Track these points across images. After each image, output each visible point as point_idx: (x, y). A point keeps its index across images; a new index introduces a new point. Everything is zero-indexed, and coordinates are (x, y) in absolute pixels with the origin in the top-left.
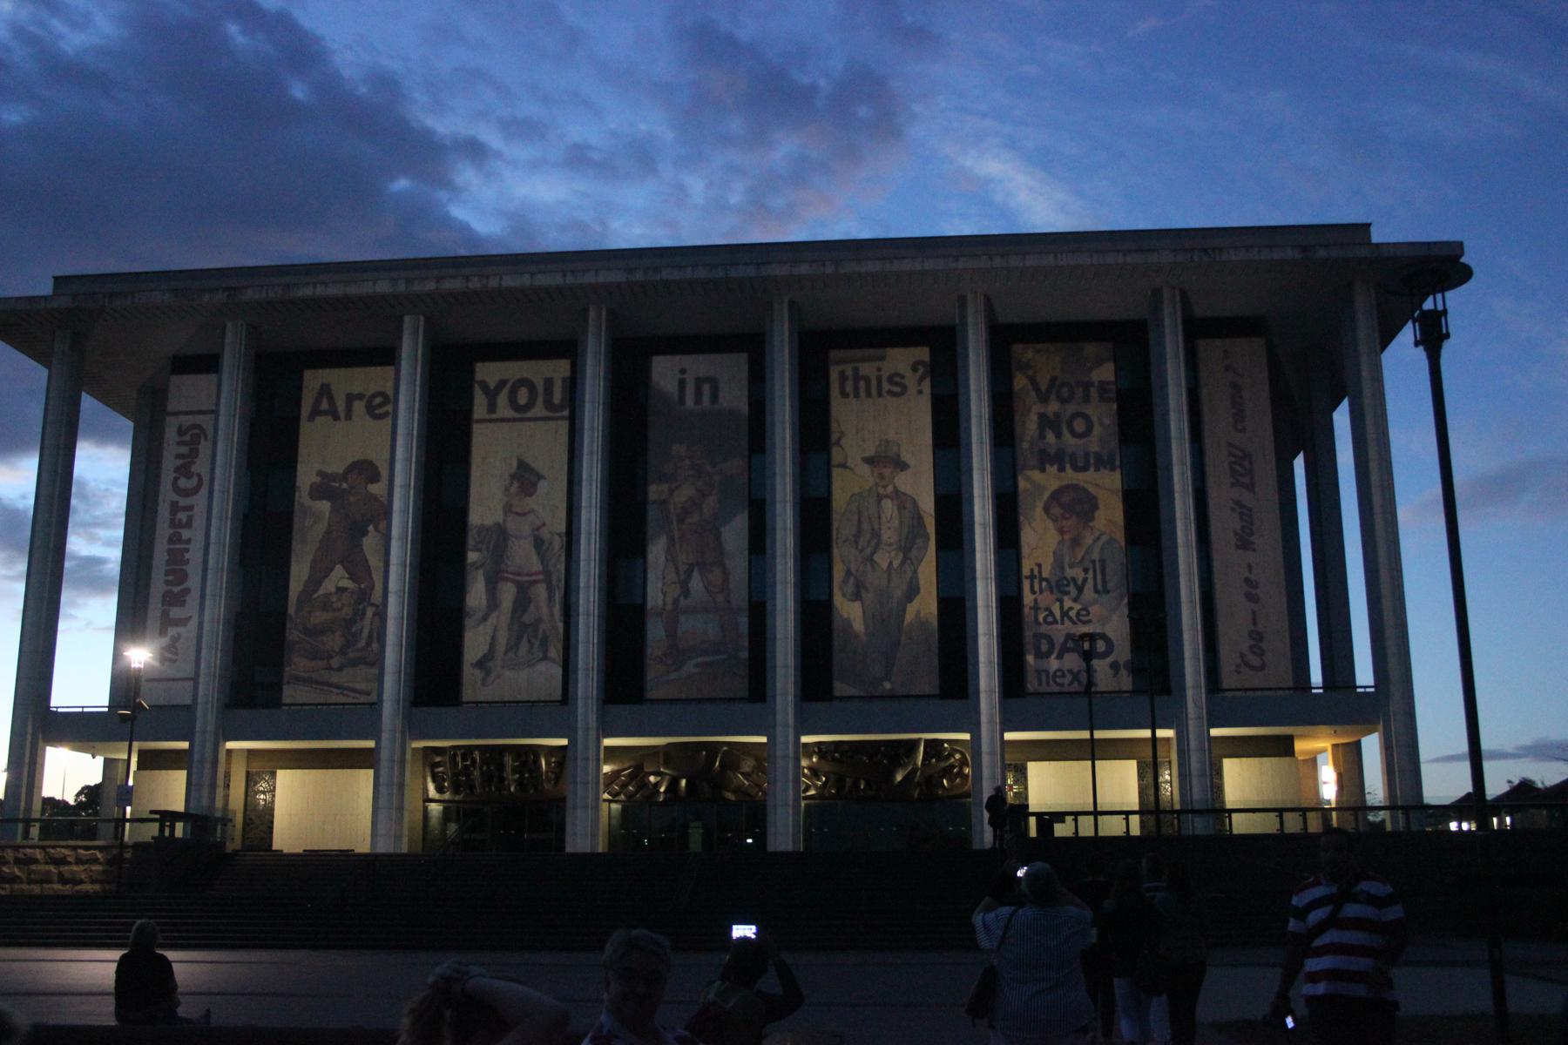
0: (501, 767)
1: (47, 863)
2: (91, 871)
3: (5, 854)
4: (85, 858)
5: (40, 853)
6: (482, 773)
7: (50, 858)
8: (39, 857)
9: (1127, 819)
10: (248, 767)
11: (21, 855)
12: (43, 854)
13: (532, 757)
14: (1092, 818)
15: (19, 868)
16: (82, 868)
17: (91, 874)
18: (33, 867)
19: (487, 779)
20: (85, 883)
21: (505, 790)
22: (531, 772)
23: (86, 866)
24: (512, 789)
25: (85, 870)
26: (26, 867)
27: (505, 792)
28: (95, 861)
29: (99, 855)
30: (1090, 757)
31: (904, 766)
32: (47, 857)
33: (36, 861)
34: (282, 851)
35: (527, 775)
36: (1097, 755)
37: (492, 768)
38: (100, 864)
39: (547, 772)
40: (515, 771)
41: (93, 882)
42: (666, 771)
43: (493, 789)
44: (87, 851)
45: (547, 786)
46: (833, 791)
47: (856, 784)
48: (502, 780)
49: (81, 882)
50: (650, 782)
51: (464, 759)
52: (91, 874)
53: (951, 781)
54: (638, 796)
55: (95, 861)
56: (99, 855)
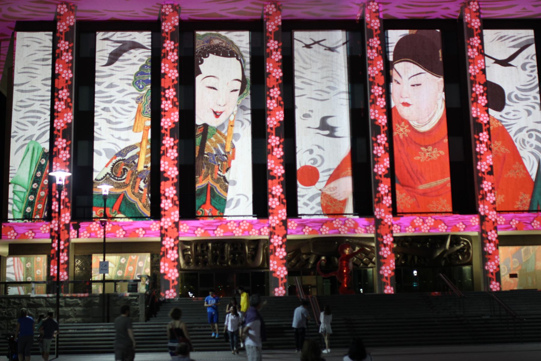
0: (223, 250)
1: (47, 307)
2: (75, 310)
3: (21, 302)
4: (71, 303)
5: (43, 301)
6: (213, 255)
7: (49, 303)
8: (42, 303)
9: (115, 285)
10: (75, 253)
11: (31, 302)
12: (45, 302)
13: (240, 246)
14: (113, 284)
15: (30, 310)
16: (70, 309)
17: (75, 312)
18: (40, 309)
19: (215, 258)
20: (72, 317)
21: (224, 263)
22: (239, 254)
23: (72, 308)
24: (229, 263)
25: (71, 310)
26: (35, 309)
27: (225, 265)
28: (77, 305)
29: (79, 302)
30: (102, 251)
31: (440, 248)
32: (47, 303)
33: (41, 306)
34: (537, 289)
35: (237, 255)
36: (107, 251)
37: (218, 252)
38: (80, 306)
39: (248, 254)
40: (231, 253)
41: (77, 316)
42: (262, 252)
43: (218, 263)
44: (72, 299)
45: (249, 261)
46: (403, 262)
47: (318, 258)
48: (223, 258)
49: (69, 317)
50: (303, 258)
51: (202, 247)
52: (75, 312)
53: (463, 256)
54: (297, 265)
55: (77, 305)
56: (79, 302)
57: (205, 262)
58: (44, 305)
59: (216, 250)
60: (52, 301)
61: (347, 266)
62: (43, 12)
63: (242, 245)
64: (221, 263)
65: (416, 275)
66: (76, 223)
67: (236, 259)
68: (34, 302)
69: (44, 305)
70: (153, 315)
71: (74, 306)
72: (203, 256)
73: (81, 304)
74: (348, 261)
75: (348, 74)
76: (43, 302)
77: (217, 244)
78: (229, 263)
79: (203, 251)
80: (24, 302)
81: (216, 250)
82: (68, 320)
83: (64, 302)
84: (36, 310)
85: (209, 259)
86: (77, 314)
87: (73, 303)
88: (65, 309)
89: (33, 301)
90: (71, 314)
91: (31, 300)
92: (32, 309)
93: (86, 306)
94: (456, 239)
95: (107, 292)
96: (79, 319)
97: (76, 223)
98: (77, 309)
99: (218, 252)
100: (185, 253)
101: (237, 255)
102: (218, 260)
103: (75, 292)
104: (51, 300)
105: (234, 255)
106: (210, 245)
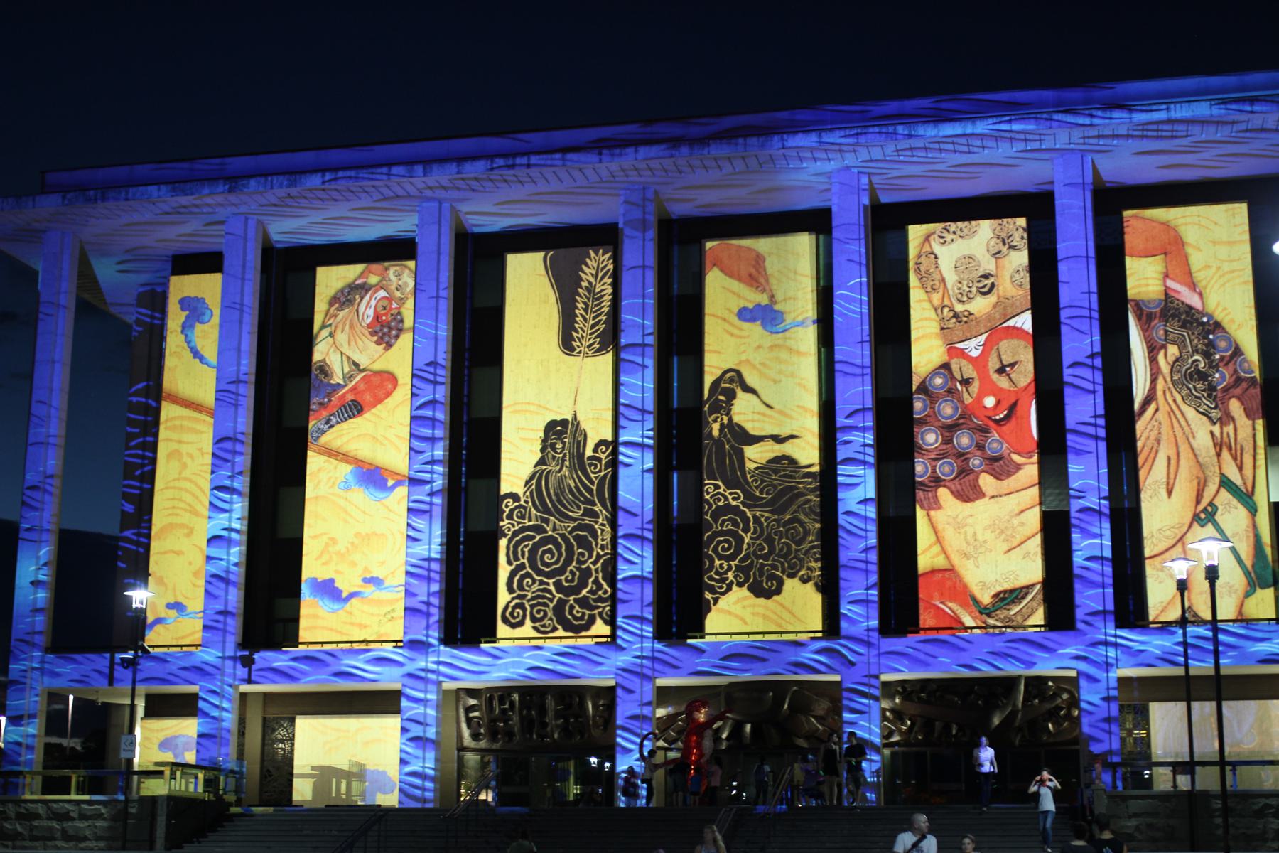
0: (543, 711)
1: (49, 819)
2: (96, 827)
3: (6, 809)
4: (89, 813)
5: (42, 807)
6: (522, 718)
7: (53, 813)
11: (23, 810)
12: (45, 810)
13: (578, 700)
15: (20, 824)
16: (86, 824)
18: (36, 823)
19: (527, 724)
20: (89, 840)
21: (547, 737)
23: (90, 822)
24: (556, 736)
25: (89, 826)
28: (99, 816)
29: (103, 810)
32: (49, 812)
33: (37, 817)
37: (533, 713)
38: (105, 819)
40: (558, 715)
41: (98, 839)
43: (535, 736)
47: (947, 727)
48: (544, 725)
49: (85, 839)
55: (99, 816)
56: (103, 810)
57: (509, 734)
58: (44, 816)
59: (529, 709)
60: (56, 808)
61: (699, 746)
62: (1244, 138)
63: (580, 697)
64: (542, 736)
65: (987, 768)
66: (247, 653)
67: (570, 728)
68: (27, 810)
69: (44, 816)
70: (195, 840)
71: (96, 819)
72: (506, 722)
73: (106, 816)
74: (701, 737)
75: (704, 294)
76: (41, 810)
77: (531, 696)
78: (556, 736)
79: (503, 711)
80: (11, 809)
81: (529, 709)
82: (83, 845)
83: (77, 812)
84: (31, 825)
85: (516, 729)
86: (99, 833)
87: (94, 812)
88: (79, 824)
89: (25, 808)
90: (87, 833)
91: (23, 805)
92: (23, 822)
93: (114, 819)
94: (1036, 684)
95: (1198, 787)
96: (102, 844)
97: (247, 653)
98: (100, 823)
99: (533, 713)
100: (471, 715)
101: (572, 720)
102: (535, 730)
103: (43, 794)
104: (55, 806)
105: (566, 721)
106: (516, 697)
